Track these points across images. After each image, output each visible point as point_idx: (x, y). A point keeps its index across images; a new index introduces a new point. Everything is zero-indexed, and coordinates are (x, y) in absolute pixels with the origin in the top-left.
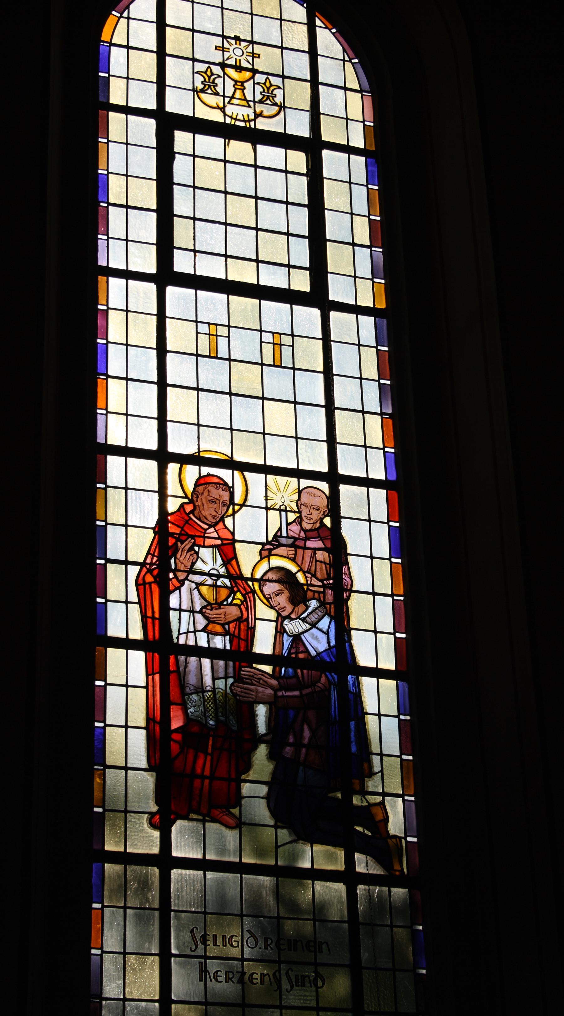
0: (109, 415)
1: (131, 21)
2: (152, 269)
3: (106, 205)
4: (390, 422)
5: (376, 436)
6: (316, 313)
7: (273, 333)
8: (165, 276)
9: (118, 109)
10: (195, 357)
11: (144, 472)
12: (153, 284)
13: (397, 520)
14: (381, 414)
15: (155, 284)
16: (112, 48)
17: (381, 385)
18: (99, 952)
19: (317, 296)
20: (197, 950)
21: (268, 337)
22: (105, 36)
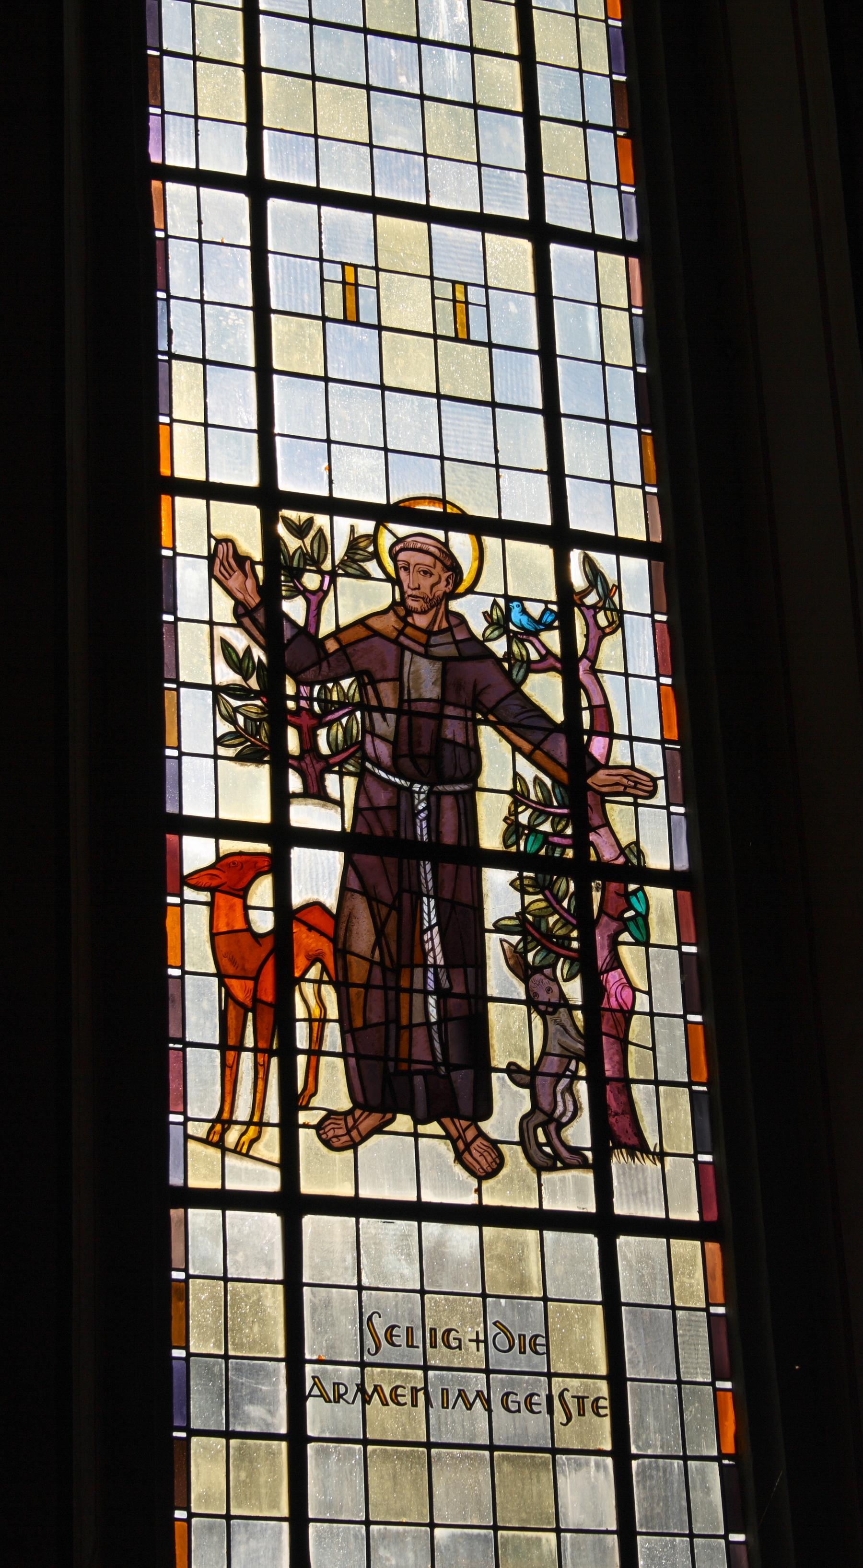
3: (157, 53)
4: (628, 142)
5: (605, 167)
7: (454, 283)
10: (323, 384)
12: (255, 507)
13: (665, 611)
14: (662, 742)
15: (258, 507)
16: (188, 1049)
21: (444, 290)
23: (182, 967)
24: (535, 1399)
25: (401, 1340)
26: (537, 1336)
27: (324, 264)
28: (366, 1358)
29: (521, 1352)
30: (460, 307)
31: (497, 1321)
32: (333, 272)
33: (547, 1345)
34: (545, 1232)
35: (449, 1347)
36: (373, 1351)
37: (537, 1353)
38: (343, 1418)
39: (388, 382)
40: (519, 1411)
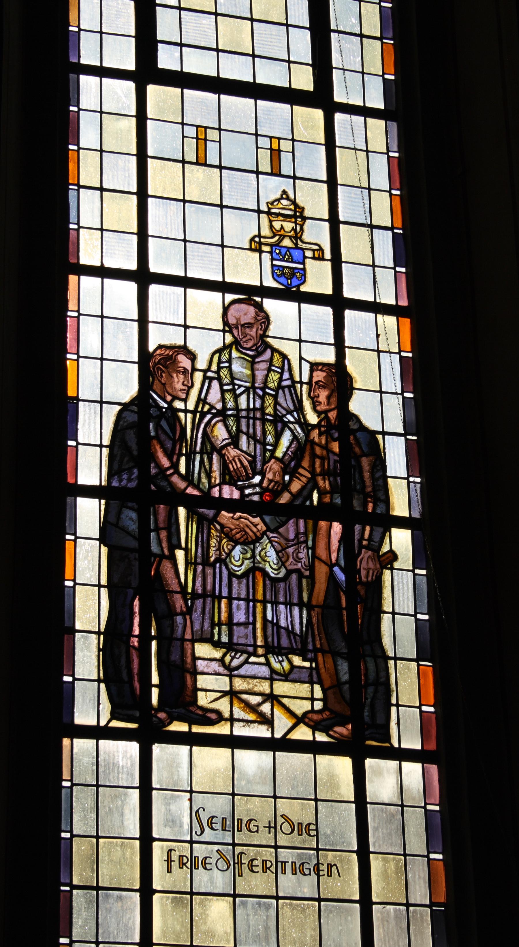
0: (81, 360)
1: (103, 115)
2: (130, 65)
6: (319, 114)
8: (146, 72)
9: (91, 70)
11: (123, 295)
17: (428, 812)
18: (76, 227)
19: (320, 96)
20: (203, 835)
22: (71, 393)
23: (74, 580)
24: (255, 863)
25: (219, 826)
26: (309, 824)
27: (369, 153)
28: (195, 838)
29: (299, 835)
30: (202, 142)
31: (284, 815)
32: (191, 132)
33: (317, 830)
34: (402, 763)
35: (250, 831)
36: (199, 833)
37: (309, 835)
38: (180, 878)
39: (105, 186)
40: (310, 874)
